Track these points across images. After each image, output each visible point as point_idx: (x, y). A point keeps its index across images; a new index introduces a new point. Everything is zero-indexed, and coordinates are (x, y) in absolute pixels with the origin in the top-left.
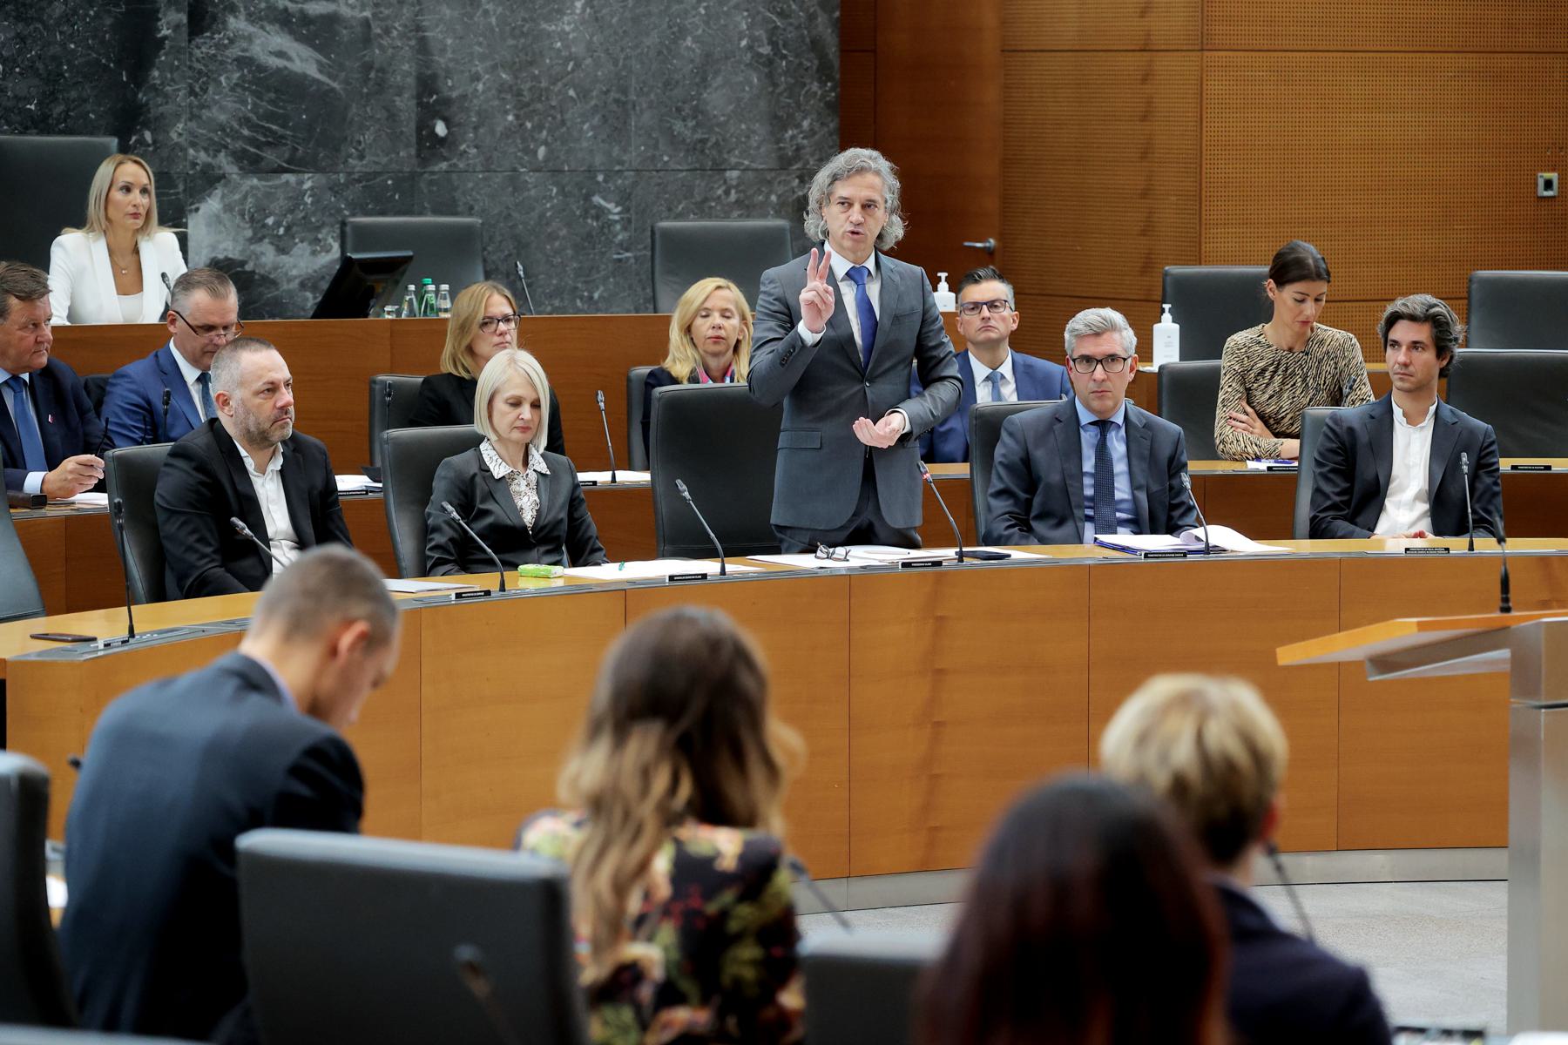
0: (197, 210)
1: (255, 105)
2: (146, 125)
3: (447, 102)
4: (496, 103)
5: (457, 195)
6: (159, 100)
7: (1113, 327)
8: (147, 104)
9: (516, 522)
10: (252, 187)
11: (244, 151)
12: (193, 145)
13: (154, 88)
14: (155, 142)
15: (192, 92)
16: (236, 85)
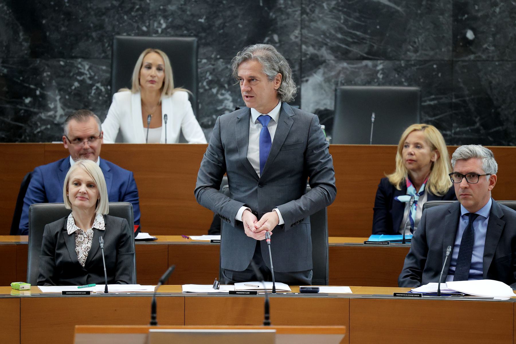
0: (307, 81)
1: (346, 21)
2: (275, 31)
3: (475, 19)
4: (508, 20)
5: (481, 74)
6: (283, 17)
7: (476, 156)
8: (275, 19)
9: (73, 259)
10: (343, 68)
11: (339, 47)
12: (306, 43)
13: (280, 10)
14: (280, 41)
15: (303, 12)
16: (334, 8)
